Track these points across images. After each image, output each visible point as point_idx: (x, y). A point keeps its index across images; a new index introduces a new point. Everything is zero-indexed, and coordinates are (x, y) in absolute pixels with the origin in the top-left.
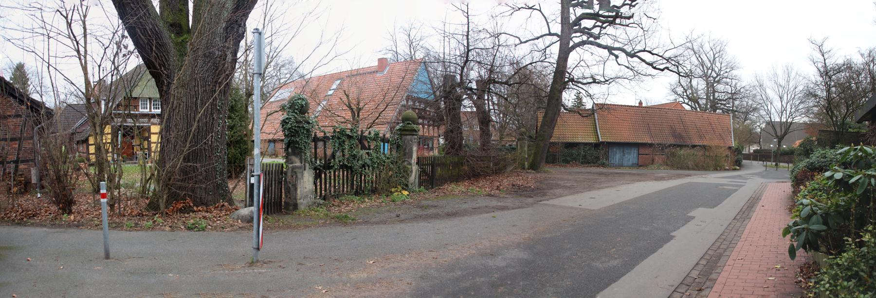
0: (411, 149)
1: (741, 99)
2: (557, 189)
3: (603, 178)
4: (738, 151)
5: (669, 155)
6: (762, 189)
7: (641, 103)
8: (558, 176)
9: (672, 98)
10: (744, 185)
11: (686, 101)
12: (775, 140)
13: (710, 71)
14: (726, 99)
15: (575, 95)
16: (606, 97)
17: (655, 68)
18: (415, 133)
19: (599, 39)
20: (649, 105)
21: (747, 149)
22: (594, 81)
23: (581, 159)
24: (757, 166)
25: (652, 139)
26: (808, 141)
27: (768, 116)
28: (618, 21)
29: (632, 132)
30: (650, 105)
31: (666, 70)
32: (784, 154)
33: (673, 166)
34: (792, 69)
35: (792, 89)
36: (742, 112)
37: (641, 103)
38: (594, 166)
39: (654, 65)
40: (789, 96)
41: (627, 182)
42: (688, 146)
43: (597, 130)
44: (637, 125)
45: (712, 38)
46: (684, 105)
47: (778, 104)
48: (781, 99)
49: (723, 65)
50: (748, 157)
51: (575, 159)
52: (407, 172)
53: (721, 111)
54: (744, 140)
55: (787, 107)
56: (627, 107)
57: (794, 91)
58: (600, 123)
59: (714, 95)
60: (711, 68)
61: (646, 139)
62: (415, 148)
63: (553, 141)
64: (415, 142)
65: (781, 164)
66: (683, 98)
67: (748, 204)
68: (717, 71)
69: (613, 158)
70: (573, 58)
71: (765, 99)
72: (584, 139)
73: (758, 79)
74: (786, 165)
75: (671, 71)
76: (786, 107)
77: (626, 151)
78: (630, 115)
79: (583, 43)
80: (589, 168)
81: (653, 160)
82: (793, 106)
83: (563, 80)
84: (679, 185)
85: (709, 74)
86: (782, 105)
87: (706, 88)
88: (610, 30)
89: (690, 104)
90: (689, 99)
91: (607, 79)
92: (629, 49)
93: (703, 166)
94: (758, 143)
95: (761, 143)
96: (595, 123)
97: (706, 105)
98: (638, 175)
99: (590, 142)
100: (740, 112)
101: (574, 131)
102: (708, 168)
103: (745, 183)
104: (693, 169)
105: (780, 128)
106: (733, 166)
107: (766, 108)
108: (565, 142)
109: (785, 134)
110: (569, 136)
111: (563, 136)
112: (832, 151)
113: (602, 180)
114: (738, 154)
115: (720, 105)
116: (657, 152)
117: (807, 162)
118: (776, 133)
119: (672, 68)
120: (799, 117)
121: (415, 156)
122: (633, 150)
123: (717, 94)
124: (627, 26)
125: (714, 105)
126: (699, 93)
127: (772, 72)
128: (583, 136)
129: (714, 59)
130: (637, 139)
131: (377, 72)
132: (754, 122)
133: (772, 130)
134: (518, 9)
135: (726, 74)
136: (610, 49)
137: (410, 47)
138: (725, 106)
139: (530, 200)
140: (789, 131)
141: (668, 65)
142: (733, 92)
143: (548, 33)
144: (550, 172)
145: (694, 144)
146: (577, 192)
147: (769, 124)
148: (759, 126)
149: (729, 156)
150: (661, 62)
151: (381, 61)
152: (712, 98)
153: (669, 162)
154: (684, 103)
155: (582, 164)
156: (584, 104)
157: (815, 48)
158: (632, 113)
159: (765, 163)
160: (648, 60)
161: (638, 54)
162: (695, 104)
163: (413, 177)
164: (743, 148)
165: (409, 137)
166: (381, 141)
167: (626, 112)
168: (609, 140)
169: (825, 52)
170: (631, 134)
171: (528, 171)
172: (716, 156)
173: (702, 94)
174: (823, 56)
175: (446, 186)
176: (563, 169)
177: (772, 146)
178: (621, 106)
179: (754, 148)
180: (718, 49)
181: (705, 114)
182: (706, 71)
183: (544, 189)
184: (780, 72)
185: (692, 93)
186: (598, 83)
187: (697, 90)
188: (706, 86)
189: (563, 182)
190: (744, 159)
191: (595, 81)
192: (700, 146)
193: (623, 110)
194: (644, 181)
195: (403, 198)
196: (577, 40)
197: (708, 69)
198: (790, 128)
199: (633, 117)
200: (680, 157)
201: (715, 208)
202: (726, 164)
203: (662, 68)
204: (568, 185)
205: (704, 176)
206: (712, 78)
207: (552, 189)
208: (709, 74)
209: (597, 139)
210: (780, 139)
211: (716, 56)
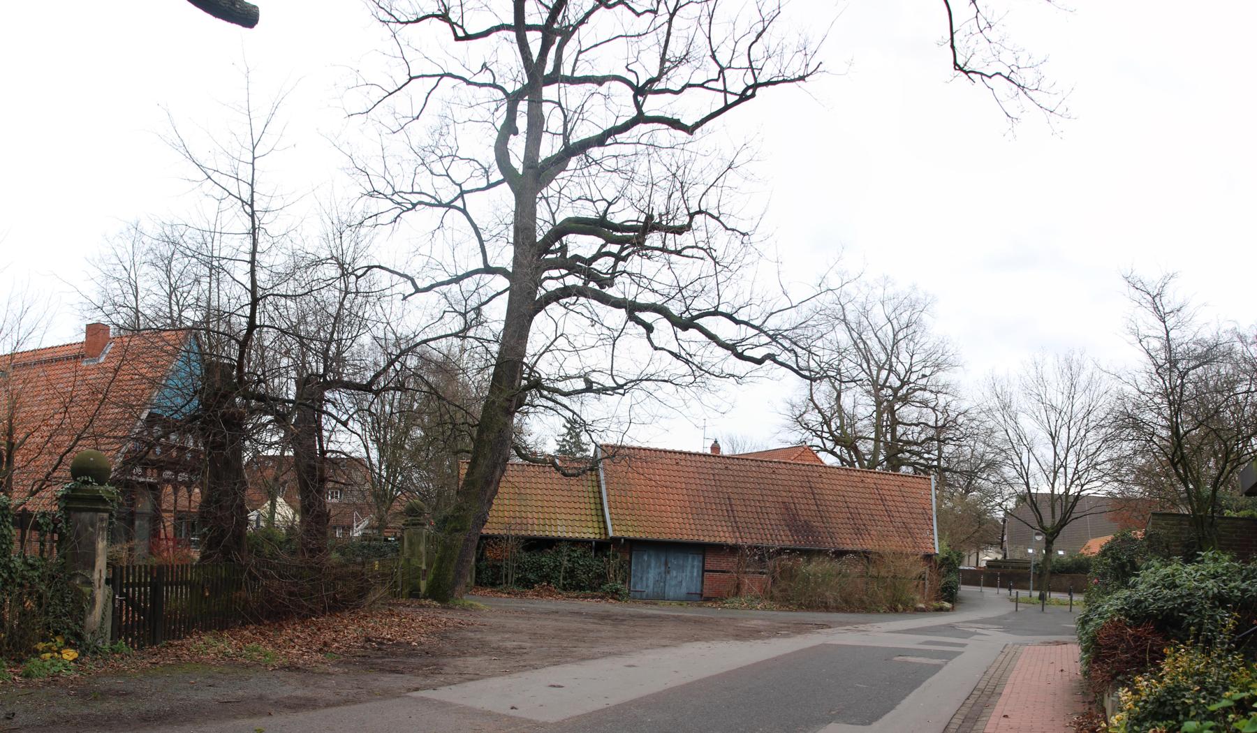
0: (93, 545)
1: (958, 439)
2: (476, 655)
3: (607, 629)
4: (947, 564)
5: (777, 575)
6: (1005, 664)
7: (716, 447)
8: (493, 620)
9: (794, 437)
10: (960, 653)
11: (829, 445)
12: (1039, 538)
13: (884, 373)
14: (923, 442)
15: (565, 426)
16: (624, 428)
17: (741, 356)
18: (101, 507)
19: (611, 285)
20: (739, 451)
21: (973, 558)
22: (589, 388)
23: (561, 578)
24: (996, 600)
25: (737, 534)
26: (1123, 540)
27: (1021, 481)
28: (654, 239)
29: (690, 517)
30: (741, 453)
31: (768, 362)
32: (1062, 572)
33: (788, 600)
34: (1081, 367)
35: (1080, 416)
36: (961, 473)
37: (716, 447)
38: (593, 598)
39: (739, 350)
40: (1073, 434)
41: (664, 642)
42: (821, 553)
43: (602, 510)
44: (702, 499)
45: (890, 291)
46: (822, 455)
47: (1044, 451)
48: (1053, 439)
49: (916, 357)
50: (973, 578)
51: (547, 578)
52: (81, 605)
53: (910, 470)
54: (964, 537)
55: (1069, 459)
56: (678, 456)
57: (1085, 421)
58: (612, 492)
59: (894, 431)
60: (887, 367)
61: (722, 534)
62: (101, 545)
63: (490, 532)
64: (103, 529)
65: (1054, 595)
66: (821, 437)
67: (965, 710)
68: (902, 373)
69: (641, 578)
70: (541, 327)
71: (1015, 439)
72: (570, 528)
73: (999, 389)
74: (1064, 597)
75: (782, 364)
76: (1066, 458)
77: (673, 561)
78: (687, 475)
79: (566, 292)
80: (579, 602)
81: (738, 587)
82: (1083, 457)
83: (516, 384)
84: (795, 653)
85: (881, 381)
86: (1055, 452)
87: (874, 415)
88: (635, 264)
89: (839, 453)
90: (837, 441)
91: (621, 382)
92: (676, 308)
93: (862, 601)
94: (998, 544)
95: (1006, 545)
96: (600, 492)
97: (875, 453)
98: (697, 622)
99: (586, 536)
100: (956, 472)
101: (546, 510)
102: (874, 607)
103: (963, 645)
104: (838, 609)
105: (1049, 509)
106: (937, 600)
107: (1017, 461)
108: (523, 537)
109: (1064, 522)
110: (536, 522)
111: (519, 521)
112: (1189, 568)
113: (603, 634)
114: (949, 571)
115: (908, 455)
116: (748, 566)
117: (1125, 599)
118: (1040, 521)
119: (784, 357)
120: (1099, 483)
121: (101, 562)
122: (690, 560)
123: (900, 430)
124: (678, 253)
125: (895, 454)
126: (859, 425)
127: (1033, 372)
128: (570, 523)
129: (896, 343)
130: (700, 532)
131: (83, 357)
132: (990, 495)
133: (1031, 513)
134: (410, 206)
135: (924, 381)
136: (632, 309)
137: (170, 298)
138: (921, 458)
139: (387, 680)
140: (1073, 516)
141: (774, 349)
142: (940, 424)
143: (482, 266)
144: (478, 609)
145: (841, 547)
146: (524, 668)
147: (1025, 500)
148: (1000, 505)
149: (927, 576)
150: (755, 341)
151: (95, 331)
152: (889, 436)
153: (776, 592)
154: (825, 450)
155: (565, 590)
156: (584, 447)
157: (1143, 301)
158: (692, 469)
159: (1014, 591)
160: (722, 337)
161: (701, 321)
162: (849, 453)
163: (98, 613)
164: (960, 558)
165: (86, 516)
166: (13, 524)
167: (676, 467)
168: (631, 535)
169: (1167, 310)
170: (686, 521)
171: (423, 602)
172: (894, 577)
173: (865, 426)
174: (1164, 322)
175: (188, 641)
176: (514, 603)
177: (1030, 551)
178: (665, 451)
179: (989, 555)
180: (904, 319)
181: (870, 475)
182: (875, 373)
183: (444, 655)
184: (1051, 374)
185: (841, 427)
186: (598, 391)
187: (852, 417)
188: (875, 408)
189: (499, 637)
190: (964, 583)
191: (592, 387)
192: (854, 552)
193: (669, 461)
194: (706, 639)
195: (57, 669)
196: (551, 286)
197: (880, 368)
198: (1076, 509)
199: (692, 481)
200: (806, 580)
201: (876, 725)
202: (918, 597)
203: (759, 357)
204: (509, 644)
205: (861, 627)
206: (890, 391)
207: (464, 654)
208: (881, 381)
209: (603, 531)
210: (1052, 534)
211: (900, 336)
